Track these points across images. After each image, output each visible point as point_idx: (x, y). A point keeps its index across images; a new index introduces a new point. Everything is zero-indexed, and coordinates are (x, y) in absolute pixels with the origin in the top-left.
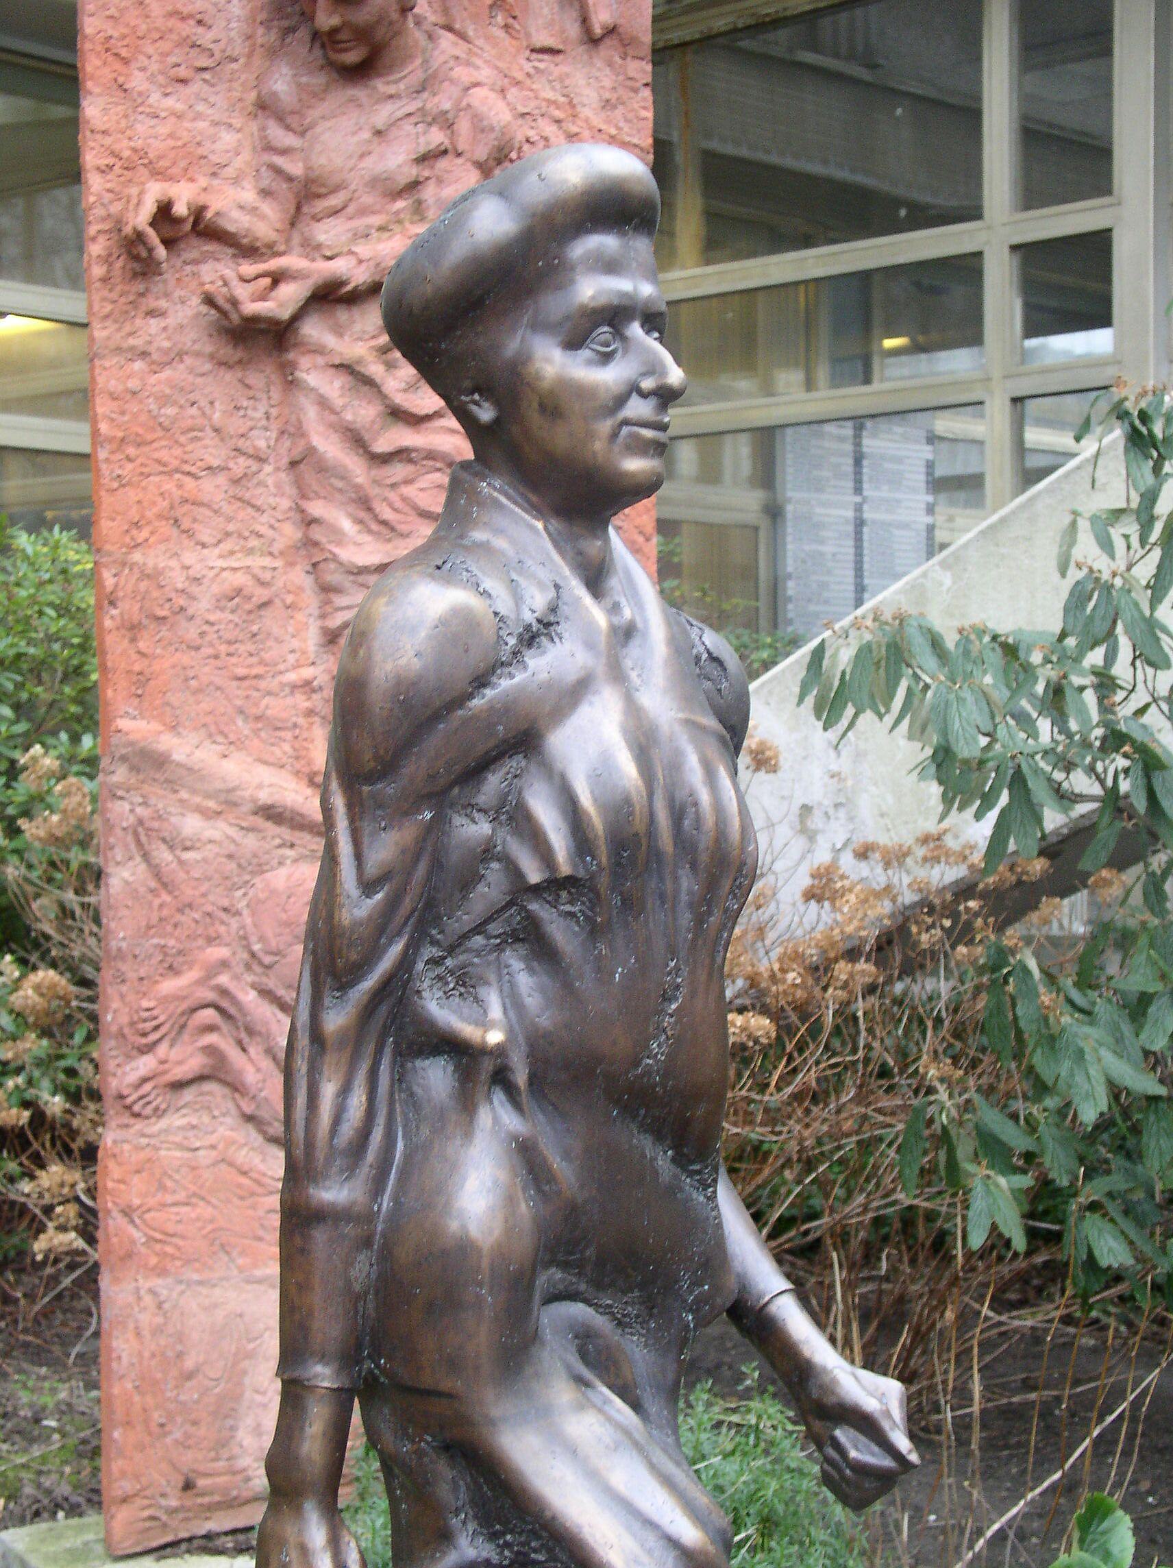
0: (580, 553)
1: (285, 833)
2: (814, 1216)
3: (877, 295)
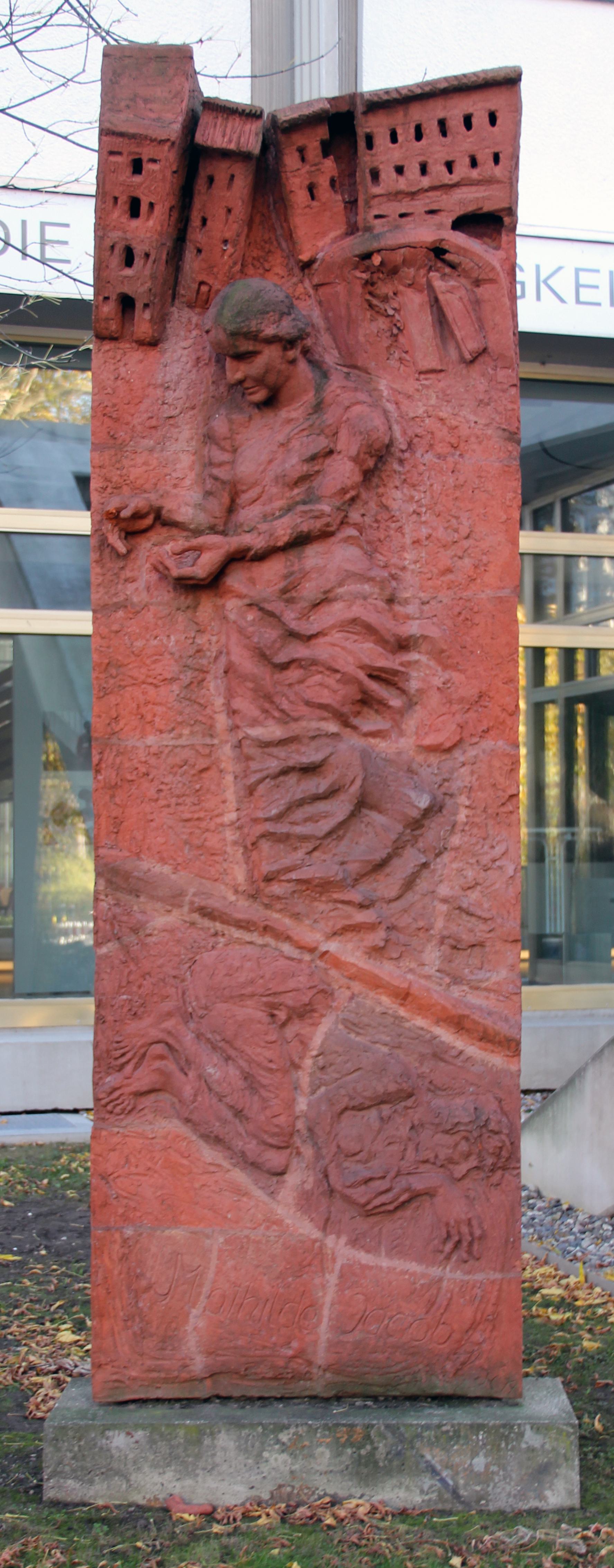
1: (218, 926)
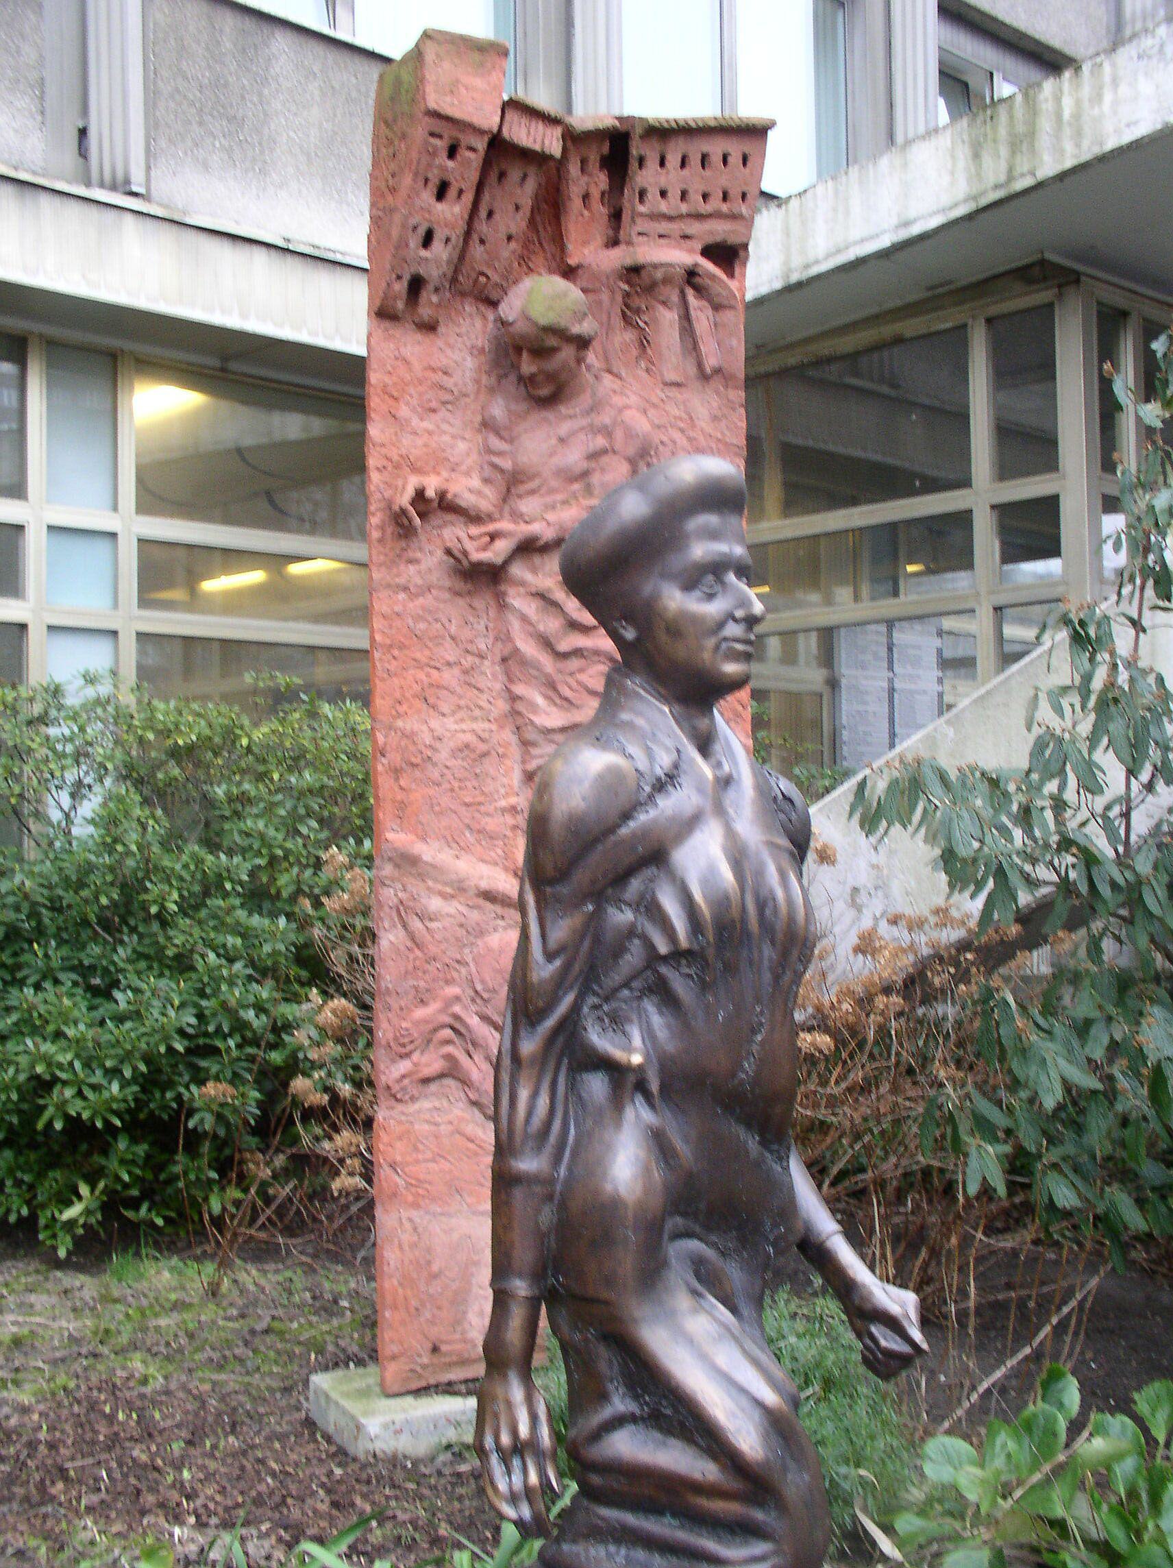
0: (694, 728)
1: (499, 909)
2: (862, 1170)
3: (902, 537)
